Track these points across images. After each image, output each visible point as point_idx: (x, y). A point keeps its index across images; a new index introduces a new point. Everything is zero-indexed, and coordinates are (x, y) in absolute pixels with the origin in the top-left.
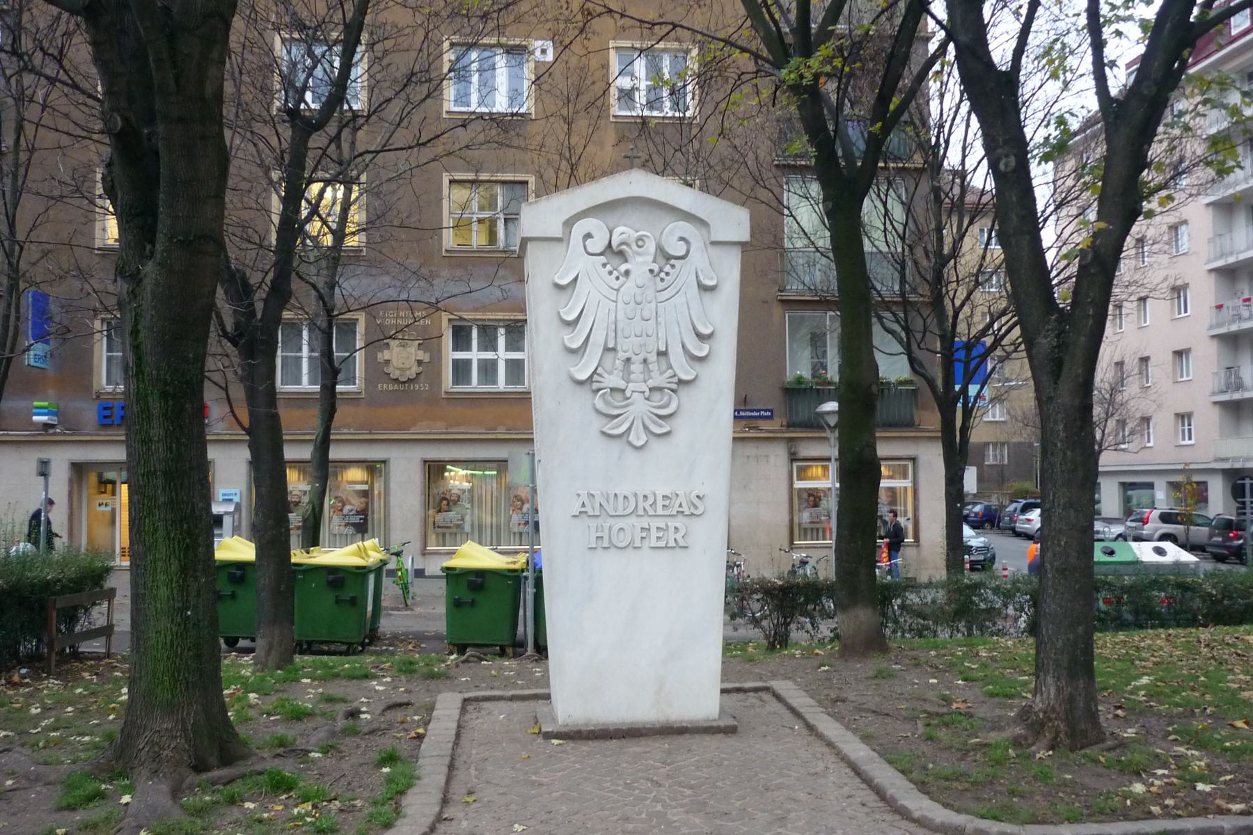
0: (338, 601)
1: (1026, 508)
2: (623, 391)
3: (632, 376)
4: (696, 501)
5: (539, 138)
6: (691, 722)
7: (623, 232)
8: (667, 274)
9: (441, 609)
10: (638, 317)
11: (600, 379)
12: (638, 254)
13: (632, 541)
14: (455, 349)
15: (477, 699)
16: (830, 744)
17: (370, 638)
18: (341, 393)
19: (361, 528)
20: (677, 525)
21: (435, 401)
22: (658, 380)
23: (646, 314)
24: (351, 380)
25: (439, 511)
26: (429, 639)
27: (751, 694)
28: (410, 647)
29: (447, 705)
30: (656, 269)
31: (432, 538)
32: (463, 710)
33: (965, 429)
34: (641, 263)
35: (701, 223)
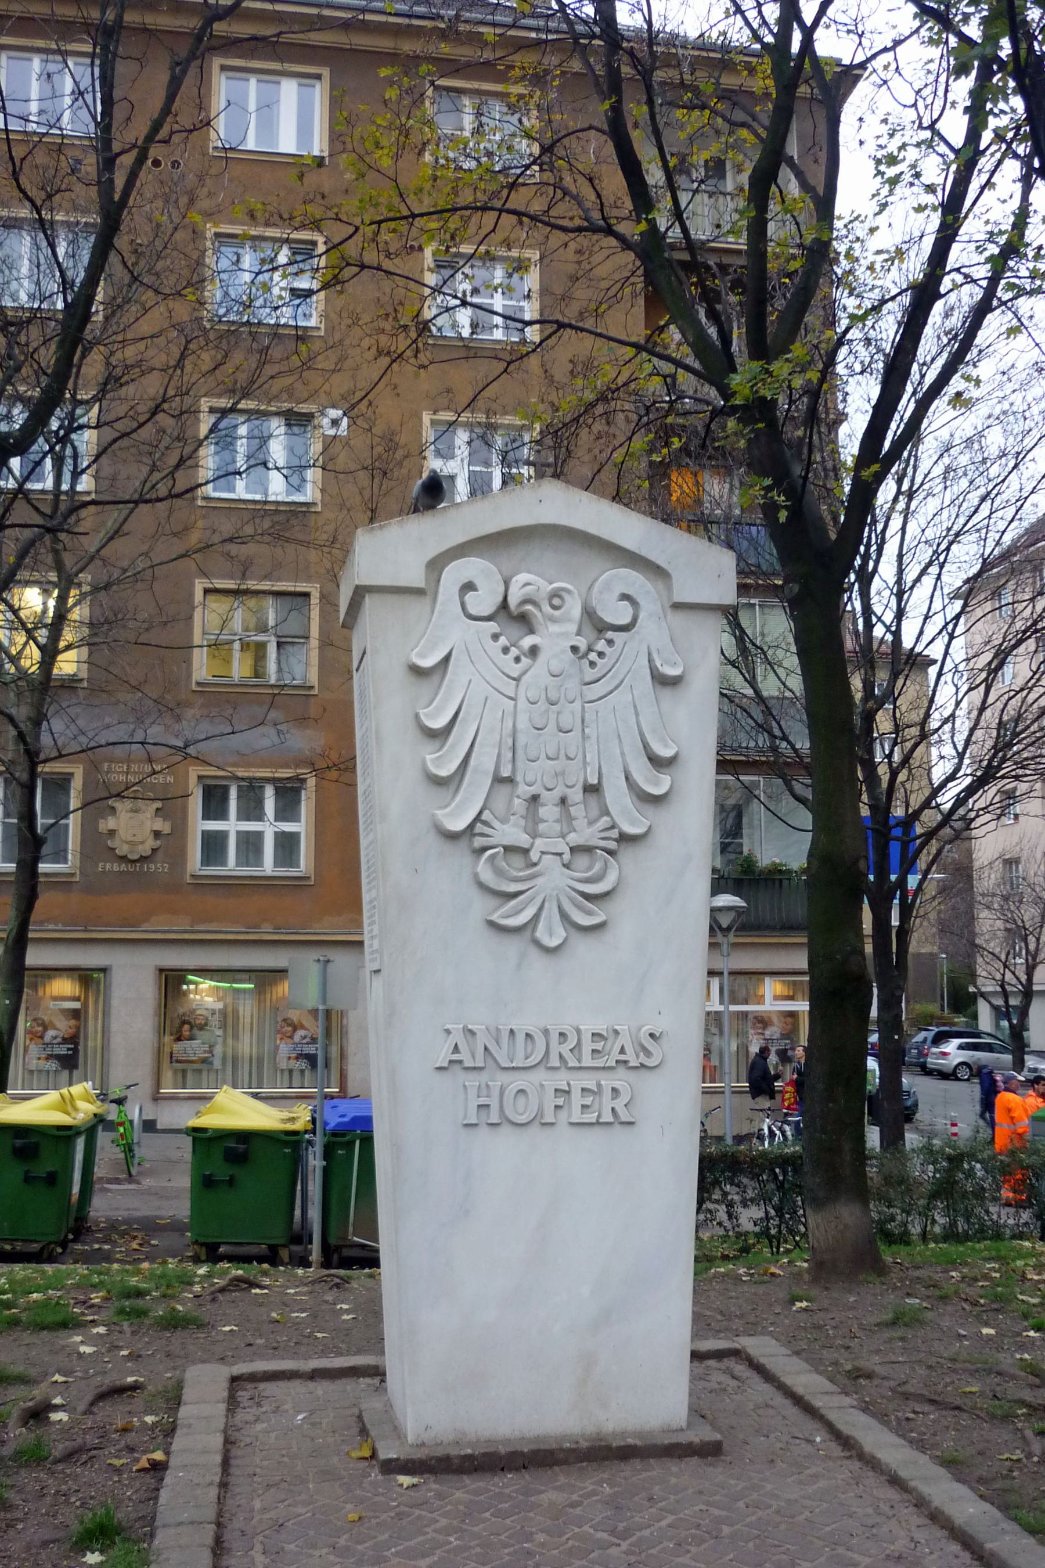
0: (28, 1179)
1: (940, 1038)
2: (526, 852)
3: (542, 827)
4: (649, 1043)
5: (330, 528)
6: (638, 1434)
7: (527, 583)
8: (601, 655)
9: (183, 1181)
10: (552, 727)
11: (487, 830)
12: (553, 620)
13: (540, 1113)
14: (206, 816)
15: (254, 1378)
16: (895, 1481)
17: (80, 1226)
18: (46, 875)
19: (69, 1061)
20: (617, 1084)
21: (179, 889)
22: (585, 834)
23: (566, 721)
24: (60, 855)
25: (179, 1039)
26: (164, 1228)
27: (712, 1363)
28: (135, 1245)
29: (204, 1386)
30: (583, 647)
31: (168, 1075)
32: (232, 1403)
33: (904, 932)
34: (557, 636)
35: (656, 571)
